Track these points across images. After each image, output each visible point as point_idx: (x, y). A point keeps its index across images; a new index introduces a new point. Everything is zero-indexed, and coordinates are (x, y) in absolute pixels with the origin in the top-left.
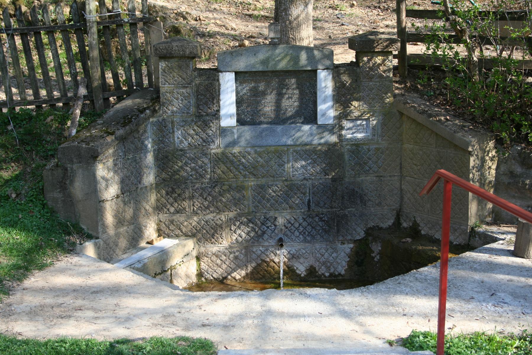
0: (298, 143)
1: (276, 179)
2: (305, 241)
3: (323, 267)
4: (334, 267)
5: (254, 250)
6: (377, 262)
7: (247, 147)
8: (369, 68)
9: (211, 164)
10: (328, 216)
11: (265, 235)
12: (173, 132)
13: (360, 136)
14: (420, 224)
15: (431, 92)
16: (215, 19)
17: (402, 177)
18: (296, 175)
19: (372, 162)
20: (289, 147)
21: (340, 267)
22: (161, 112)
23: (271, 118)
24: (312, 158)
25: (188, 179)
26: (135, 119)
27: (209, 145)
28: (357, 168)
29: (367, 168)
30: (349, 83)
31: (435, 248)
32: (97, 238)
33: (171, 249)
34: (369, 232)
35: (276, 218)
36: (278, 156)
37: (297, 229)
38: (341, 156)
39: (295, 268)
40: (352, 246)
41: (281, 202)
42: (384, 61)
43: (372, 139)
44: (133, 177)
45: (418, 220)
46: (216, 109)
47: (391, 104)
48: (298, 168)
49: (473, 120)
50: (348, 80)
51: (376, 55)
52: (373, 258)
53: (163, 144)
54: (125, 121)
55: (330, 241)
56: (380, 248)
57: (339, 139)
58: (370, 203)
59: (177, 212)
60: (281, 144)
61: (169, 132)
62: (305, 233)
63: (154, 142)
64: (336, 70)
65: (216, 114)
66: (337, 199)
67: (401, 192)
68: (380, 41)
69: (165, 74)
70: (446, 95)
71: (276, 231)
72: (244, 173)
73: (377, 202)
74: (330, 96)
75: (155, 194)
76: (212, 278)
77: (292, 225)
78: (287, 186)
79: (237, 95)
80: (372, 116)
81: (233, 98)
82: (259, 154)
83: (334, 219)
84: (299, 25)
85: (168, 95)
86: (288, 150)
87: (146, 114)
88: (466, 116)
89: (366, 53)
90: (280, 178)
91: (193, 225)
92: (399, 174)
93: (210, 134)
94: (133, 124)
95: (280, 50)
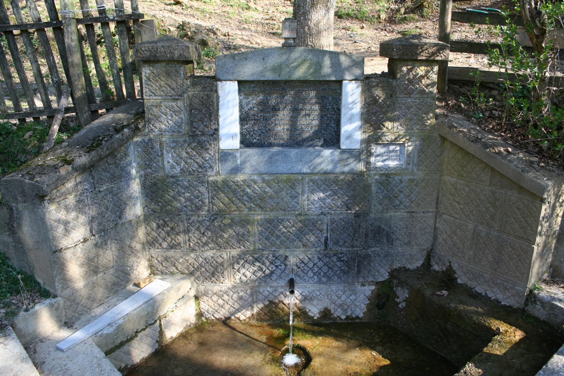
0: (316, 171)
1: (287, 213)
2: (320, 282)
4: (351, 310)
5: (261, 290)
6: (402, 309)
7: (252, 174)
8: (409, 80)
9: (208, 193)
10: (348, 256)
11: (274, 275)
12: (162, 154)
13: (392, 164)
15: (479, 114)
16: (242, 35)
17: (437, 214)
18: (311, 208)
22: (147, 130)
24: (331, 190)
26: (106, 141)
27: (206, 171)
28: (386, 202)
29: (398, 203)
30: (382, 98)
32: (55, 296)
34: (394, 274)
35: (286, 257)
36: (290, 186)
37: (310, 269)
38: (367, 187)
39: (308, 310)
40: (373, 288)
41: (292, 239)
42: (427, 72)
43: (406, 169)
45: (455, 266)
46: (214, 127)
47: (432, 127)
48: (314, 200)
49: (540, 152)
50: (381, 95)
51: (418, 64)
53: (151, 169)
54: (92, 144)
56: (407, 296)
57: (366, 168)
58: (398, 242)
59: (172, 247)
60: (294, 172)
61: (158, 155)
62: (320, 274)
63: (141, 167)
64: (367, 81)
65: (214, 133)
66: (359, 237)
67: (435, 230)
69: (150, 83)
70: (500, 118)
71: (287, 271)
72: (249, 205)
73: (406, 241)
74: (357, 114)
75: (143, 226)
76: (213, 318)
77: (305, 264)
78: (300, 221)
81: (236, 114)
83: (355, 259)
84: (319, 32)
85: (154, 109)
86: (303, 179)
87: (122, 135)
88: (530, 148)
91: (189, 262)
92: (435, 210)
93: (207, 158)
94: (102, 149)
95: (297, 53)
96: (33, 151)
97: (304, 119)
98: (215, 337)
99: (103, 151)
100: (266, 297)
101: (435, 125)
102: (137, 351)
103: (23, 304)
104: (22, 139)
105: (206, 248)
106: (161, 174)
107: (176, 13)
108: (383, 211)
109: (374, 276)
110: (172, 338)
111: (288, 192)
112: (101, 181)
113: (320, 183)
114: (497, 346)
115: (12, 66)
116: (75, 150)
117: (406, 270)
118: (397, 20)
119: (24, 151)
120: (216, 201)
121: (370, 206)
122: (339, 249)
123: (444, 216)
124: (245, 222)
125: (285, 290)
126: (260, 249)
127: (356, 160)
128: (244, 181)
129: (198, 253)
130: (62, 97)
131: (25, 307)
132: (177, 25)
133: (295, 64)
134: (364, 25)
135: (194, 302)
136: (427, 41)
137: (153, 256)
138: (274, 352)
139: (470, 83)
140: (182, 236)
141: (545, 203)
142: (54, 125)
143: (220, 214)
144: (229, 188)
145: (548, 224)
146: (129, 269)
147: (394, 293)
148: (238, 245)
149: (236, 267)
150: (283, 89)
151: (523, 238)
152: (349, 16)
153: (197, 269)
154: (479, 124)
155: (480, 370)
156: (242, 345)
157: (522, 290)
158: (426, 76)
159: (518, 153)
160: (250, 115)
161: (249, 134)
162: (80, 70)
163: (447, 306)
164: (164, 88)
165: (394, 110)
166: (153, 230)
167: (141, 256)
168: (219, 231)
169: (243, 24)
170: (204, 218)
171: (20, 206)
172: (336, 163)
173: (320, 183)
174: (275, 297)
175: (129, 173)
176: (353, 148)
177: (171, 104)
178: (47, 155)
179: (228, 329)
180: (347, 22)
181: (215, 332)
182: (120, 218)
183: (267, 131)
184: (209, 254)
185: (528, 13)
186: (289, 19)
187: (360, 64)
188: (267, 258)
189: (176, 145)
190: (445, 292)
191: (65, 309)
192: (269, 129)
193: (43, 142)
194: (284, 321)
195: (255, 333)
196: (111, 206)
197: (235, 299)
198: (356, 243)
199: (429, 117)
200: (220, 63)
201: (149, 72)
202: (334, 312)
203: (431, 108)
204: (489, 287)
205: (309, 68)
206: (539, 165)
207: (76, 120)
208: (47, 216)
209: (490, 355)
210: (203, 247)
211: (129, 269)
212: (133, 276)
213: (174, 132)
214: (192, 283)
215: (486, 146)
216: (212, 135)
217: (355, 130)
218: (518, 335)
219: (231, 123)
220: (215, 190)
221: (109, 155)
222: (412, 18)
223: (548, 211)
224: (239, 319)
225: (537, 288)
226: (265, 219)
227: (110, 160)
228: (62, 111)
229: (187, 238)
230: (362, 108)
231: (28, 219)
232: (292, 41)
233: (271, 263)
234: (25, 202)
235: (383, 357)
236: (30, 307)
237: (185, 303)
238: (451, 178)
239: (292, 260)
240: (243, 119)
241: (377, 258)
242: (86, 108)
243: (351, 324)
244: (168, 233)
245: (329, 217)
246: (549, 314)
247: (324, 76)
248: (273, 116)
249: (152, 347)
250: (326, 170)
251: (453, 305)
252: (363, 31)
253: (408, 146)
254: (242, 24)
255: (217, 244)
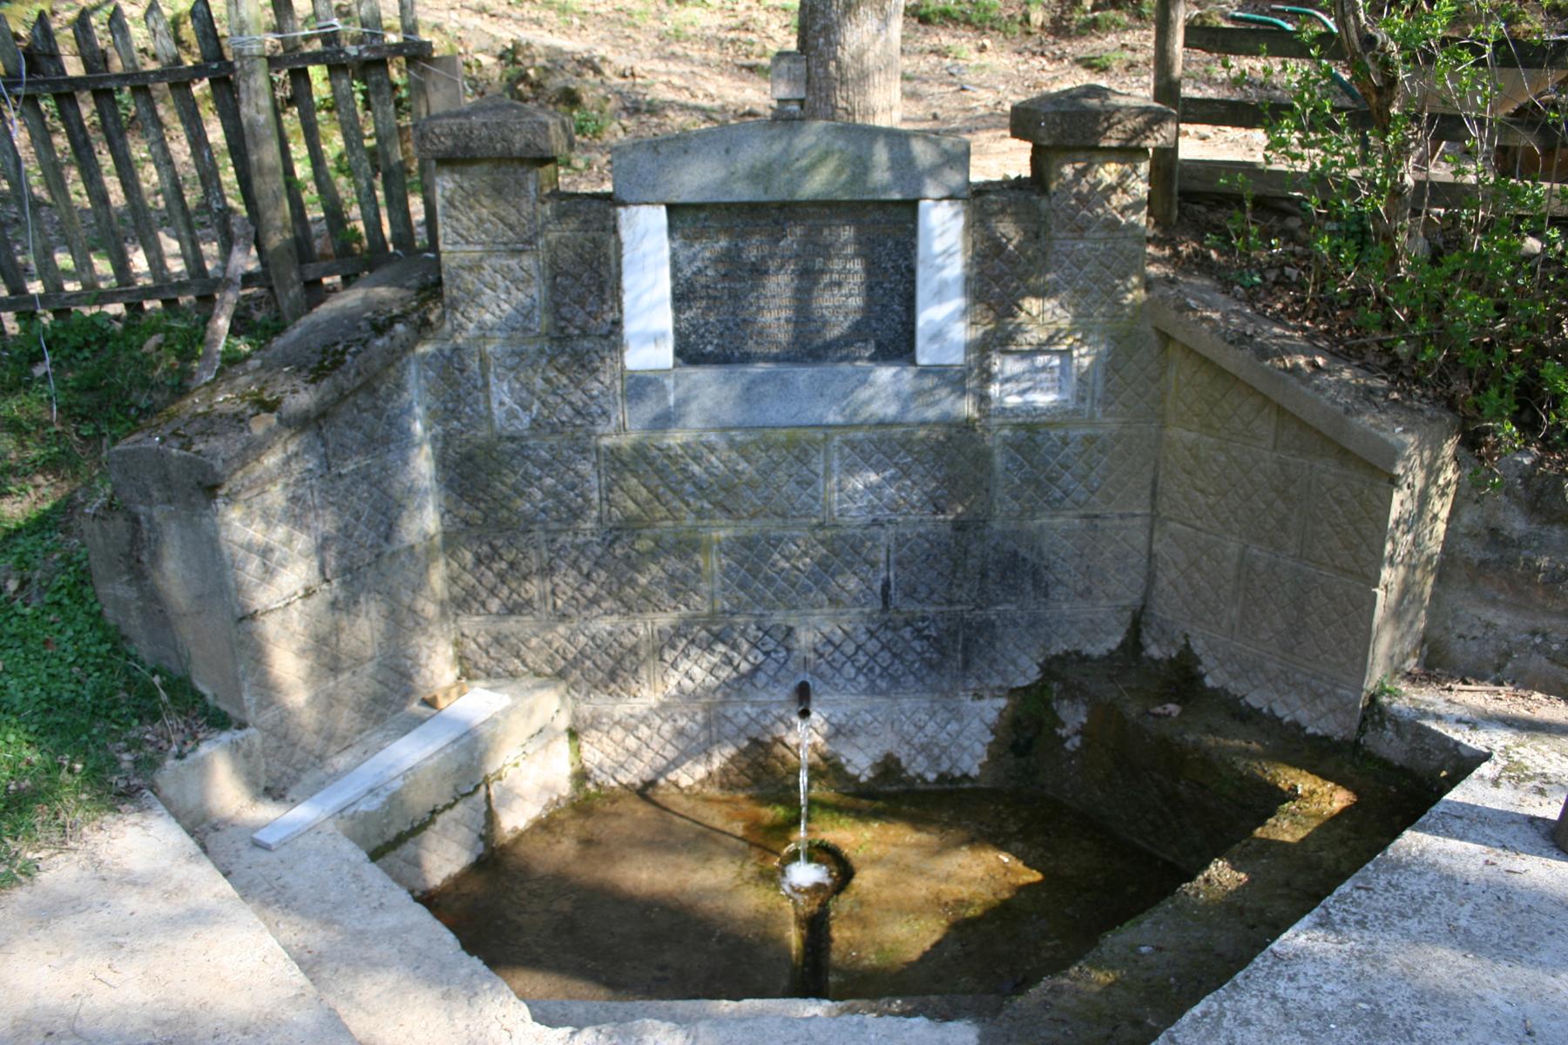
0: (858, 420)
1: (790, 522)
2: (872, 690)
3: (920, 759)
4: (950, 758)
5: (730, 713)
6: (1074, 754)
7: (705, 430)
8: (1078, 196)
9: (599, 477)
10: (941, 625)
11: (761, 675)
12: (486, 385)
13: (1043, 399)
14: (1203, 658)
15: (1252, 276)
16: (669, 73)
17: (1155, 520)
18: (848, 510)
19: (1073, 475)
20: (830, 431)
21: (966, 758)
22: (448, 326)
23: (777, 344)
24: (896, 464)
25: (533, 522)
26: (354, 355)
27: (593, 423)
28: (1029, 492)
29: (1058, 494)
30: (1015, 242)
31: (1254, 746)
32: (242, 726)
33: (483, 729)
34: (1053, 667)
35: (790, 631)
36: (797, 458)
37: (849, 658)
38: (983, 458)
39: (843, 761)
40: (1002, 703)
41: (803, 586)
42: (1123, 176)
43: (1076, 412)
44: (362, 527)
45: (1198, 646)
46: (610, 317)
47: (1138, 308)
48: (856, 491)
49: (1394, 367)
50: (1012, 234)
51: (1099, 158)
52: (1063, 740)
53: (458, 420)
54: (321, 363)
55: (943, 692)
56: (1084, 720)
57: (980, 410)
58: (1060, 589)
59: (512, 610)
60: (805, 422)
61: (475, 387)
62: (871, 670)
63: (433, 416)
64: (977, 202)
65: (611, 332)
66: (965, 578)
67: (1149, 561)
68: (1118, 116)
69: (454, 213)
70: (1302, 286)
71: (791, 665)
72: (699, 504)
73: (1080, 587)
74: (955, 281)
75: (442, 561)
76: (613, 783)
77: (837, 647)
78: (822, 542)
79: (674, 276)
80: (1082, 342)
81: (662, 286)
82: (742, 450)
83: (956, 633)
84: (864, 76)
85: (465, 275)
86: (827, 438)
87: (392, 338)
88: (1370, 358)
89: (1067, 150)
90: (804, 520)
91: (556, 645)
92: (1148, 511)
93: (595, 393)
94: (345, 373)
95: (812, 134)
96: (169, 382)
97: (827, 295)
98: (622, 826)
99: (345, 378)
100: (742, 730)
101: (1144, 304)
102: (434, 858)
103: (170, 741)
104: (138, 354)
105: (596, 610)
106: (483, 433)
107: (493, 16)
108: (1022, 513)
109: (1003, 674)
110: (515, 830)
111: (793, 470)
112: (343, 451)
113: (868, 448)
114: (1286, 824)
115: (109, 173)
116: (281, 378)
117: (1083, 659)
118: (1073, 27)
119: (146, 384)
120: (617, 495)
121: (992, 503)
122: (918, 609)
123: (1172, 525)
124: (687, 547)
125: (789, 711)
126: (724, 612)
127: (953, 392)
128: (685, 446)
129: (575, 625)
130: (235, 248)
131: (175, 749)
132: (499, 50)
133: (804, 162)
134: (987, 42)
135: (567, 745)
136: (1122, 101)
137: (467, 632)
138: (764, 859)
139: (1230, 200)
140: (535, 582)
141: (1400, 488)
142: (218, 317)
143: (630, 527)
144: (650, 464)
145: (1410, 537)
146: (409, 663)
147: (1054, 714)
148: (673, 604)
149: (669, 655)
150: (776, 222)
151: (1352, 572)
152: (947, 18)
153: (574, 663)
154: (1251, 300)
155: (1242, 876)
156: (685, 845)
157: (1352, 696)
158: (1121, 185)
159: (1341, 370)
160: (697, 285)
161: (696, 332)
162: (279, 182)
163: (1178, 739)
164: (488, 225)
165: (1044, 270)
166: (464, 568)
167: (437, 632)
168: (625, 568)
169: (669, 44)
170: (589, 537)
171: (158, 512)
172: (906, 400)
173: (868, 448)
174: (765, 729)
175: (406, 433)
176: (947, 362)
177: (505, 262)
178: (213, 391)
179: (651, 808)
180: (942, 33)
181: (618, 815)
182: (387, 539)
183: (737, 325)
184: (604, 625)
185: (1354, 36)
186: (788, 54)
187: (961, 159)
188: (743, 633)
189: (519, 360)
190: (1173, 708)
191: (266, 756)
192: (744, 321)
193: (190, 359)
194: (787, 788)
195: (715, 817)
196: (366, 510)
197: (667, 736)
198: (957, 593)
199: (1129, 285)
200: (624, 162)
201: (450, 185)
202: (909, 764)
203: (1133, 264)
204: (1278, 691)
205: (838, 171)
206: (1386, 397)
207: (267, 303)
208: (223, 534)
209: (1268, 844)
210: (586, 608)
211: (409, 663)
212: (419, 681)
213: (513, 329)
214: (562, 698)
215: (1263, 353)
216: (606, 337)
217: (950, 318)
218: (1339, 799)
219: (652, 307)
220: (615, 469)
221: (359, 388)
222: (1113, 21)
223: (1409, 505)
224: (676, 784)
225: (1389, 691)
226: (737, 538)
227: (362, 400)
228: (235, 284)
229: (548, 587)
230: (966, 266)
231: (177, 543)
232: (795, 107)
233: (754, 646)
234: (170, 501)
235: (1025, 864)
236: (186, 749)
237: (546, 747)
238: (1185, 433)
239: (805, 638)
240: (681, 298)
241: (1010, 629)
242: (294, 275)
243: (951, 792)
244: (502, 577)
245: (892, 530)
246: (1413, 749)
247: (874, 190)
248: (752, 289)
249: (472, 850)
250: (881, 415)
251: (1190, 737)
252: (986, 58)
253: (1081, 356)
254: (668, 45)
255: (622, 601)
